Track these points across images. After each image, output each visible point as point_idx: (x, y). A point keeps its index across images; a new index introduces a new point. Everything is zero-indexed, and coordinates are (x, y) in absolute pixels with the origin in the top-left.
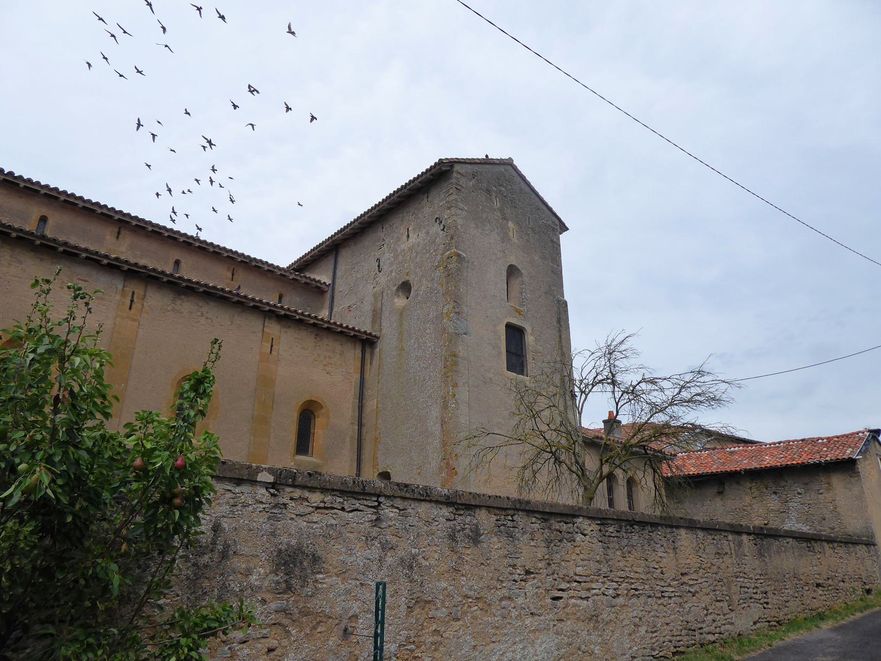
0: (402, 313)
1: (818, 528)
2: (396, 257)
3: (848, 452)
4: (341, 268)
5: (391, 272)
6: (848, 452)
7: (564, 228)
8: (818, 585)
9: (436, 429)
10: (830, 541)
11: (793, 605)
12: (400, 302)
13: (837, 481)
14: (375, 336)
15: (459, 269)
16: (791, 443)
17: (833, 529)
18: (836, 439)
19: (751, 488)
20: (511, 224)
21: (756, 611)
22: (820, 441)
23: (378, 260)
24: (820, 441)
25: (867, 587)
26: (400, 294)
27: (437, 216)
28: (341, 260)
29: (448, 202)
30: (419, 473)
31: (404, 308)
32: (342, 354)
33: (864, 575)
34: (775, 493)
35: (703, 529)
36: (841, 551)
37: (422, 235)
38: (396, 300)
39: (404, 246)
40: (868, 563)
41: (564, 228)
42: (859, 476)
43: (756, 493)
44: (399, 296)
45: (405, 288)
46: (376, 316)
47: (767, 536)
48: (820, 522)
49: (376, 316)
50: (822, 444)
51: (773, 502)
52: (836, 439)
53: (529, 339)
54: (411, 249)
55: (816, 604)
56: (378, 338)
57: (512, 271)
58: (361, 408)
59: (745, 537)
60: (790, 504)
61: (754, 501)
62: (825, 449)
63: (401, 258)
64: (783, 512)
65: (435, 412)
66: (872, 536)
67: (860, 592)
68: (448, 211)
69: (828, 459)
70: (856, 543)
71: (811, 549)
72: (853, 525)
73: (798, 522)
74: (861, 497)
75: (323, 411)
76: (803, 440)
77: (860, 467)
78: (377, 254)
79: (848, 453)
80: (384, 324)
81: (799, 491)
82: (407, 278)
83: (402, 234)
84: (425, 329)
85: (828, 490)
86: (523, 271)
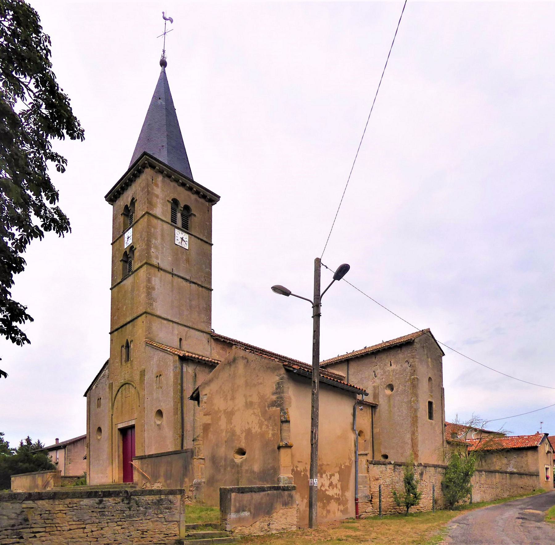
0: (389, 397)
1: (520, 470)
2: (385, 372)
3: (536, 443)
4: (351, 371)
5: (383, 378)
6: (536, 443)
7: (444, 355)
8: (522, 488)
9: (409, 441)
10: (526, 475)
11: (516, 492)
12: (388, 392)
13: (530, 453)
14: (376, 404)
15: (417, 383)
16: (513, 437)
17: (525, 470)
18: (531, 437)
19: (497, 456)
20: (429, 360)
21: (508, 493)
22: (525, 437)
23: (374, 371)
24: (525, 437)
25: (534, 489)
26: (387, 388)
27: (406, 360)
28: (350, 367)
29: (412, 355)
30: (401, 456)
31: (390, 395)
32: (366, 412)
33: (534, 486)
34: (506, 458)
35: (501, 473)
36: (529, 478)
37: (399, 366)
38: (386, 391)
39: (389, 368)
40: (536, 482)
41: (444, 355)
42: (538, 452)
43: (498, 457)
44: (386, 389)
45: (391, 387)
46: (376, 396)
47: (512, 474)
48: (521, 468)
49: (376, 396)
50: (526, 438)
51: (505, 461)
52: (531, 437)
53: (434, 406)
54: (393, 371)
55: (521, 493)
56: (378, 405)
57: (430, 379)
58: (372, 432)
59: (508, 474)
60: (511, 462)
61: (498, 460)
62: (527, 441)
63: (387, 373)
64: (508, 465)
65: (409, 436)
66: (538, 473)
67: (532, 490)
68: (412, 359)
69: (528, 446)
70: (533, 475)
71: (521, 477)
72: (532, 469)
73: (512, 468)
74: (537, 460)
75: (363, 434)
76: (518, 436)
77: (539, 449)
78: (374, 369)
79: (536, 443)
80: (380, 400)
81: (515, 457)
82: (391, 383)
83: (387, 363)
84: (402, 406)
85: (526, 457)
86: (432, 379)
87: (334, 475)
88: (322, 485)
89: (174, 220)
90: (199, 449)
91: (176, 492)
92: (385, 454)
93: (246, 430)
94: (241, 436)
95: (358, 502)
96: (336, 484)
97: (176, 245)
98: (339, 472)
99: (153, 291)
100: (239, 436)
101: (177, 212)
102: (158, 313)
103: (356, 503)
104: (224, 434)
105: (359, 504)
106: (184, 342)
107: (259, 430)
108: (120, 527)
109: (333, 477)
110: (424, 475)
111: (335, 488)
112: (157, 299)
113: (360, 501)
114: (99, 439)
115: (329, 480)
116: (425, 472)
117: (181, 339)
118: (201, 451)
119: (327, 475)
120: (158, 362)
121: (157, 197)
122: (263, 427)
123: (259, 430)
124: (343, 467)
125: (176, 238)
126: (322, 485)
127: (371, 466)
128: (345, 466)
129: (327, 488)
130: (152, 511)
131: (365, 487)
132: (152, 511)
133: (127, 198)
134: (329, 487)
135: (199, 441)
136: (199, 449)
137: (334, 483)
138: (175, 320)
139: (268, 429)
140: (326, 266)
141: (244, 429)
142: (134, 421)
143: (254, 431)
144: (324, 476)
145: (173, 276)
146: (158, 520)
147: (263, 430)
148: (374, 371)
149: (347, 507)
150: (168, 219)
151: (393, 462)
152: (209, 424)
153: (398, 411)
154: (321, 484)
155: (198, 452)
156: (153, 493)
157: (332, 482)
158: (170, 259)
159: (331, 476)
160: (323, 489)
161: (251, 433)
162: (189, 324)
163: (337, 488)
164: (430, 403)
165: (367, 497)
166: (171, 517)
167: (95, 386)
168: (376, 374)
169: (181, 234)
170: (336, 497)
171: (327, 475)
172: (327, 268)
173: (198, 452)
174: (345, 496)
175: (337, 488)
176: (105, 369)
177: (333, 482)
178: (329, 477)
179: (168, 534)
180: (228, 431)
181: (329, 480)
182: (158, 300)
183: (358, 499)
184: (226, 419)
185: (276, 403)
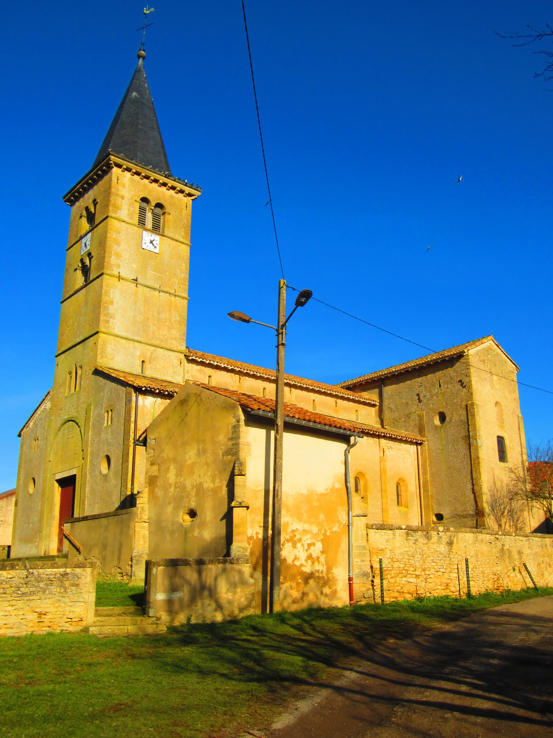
23: (418, 395)
87: (313, 544)
88: (296, 558)
89: (142, 222)
90: (143, 509)
91: (86, 565)
92: (439, 513)
93: (197, 484)
94: (191, 493)
95: (352, 583)
96: (318, 558)
97: (143, 249)
98: (322, 541)
99: (110, 306)
100: (189, 492)
101: (147, 212)
102: (116, 332)
103: (349, 583)
104: (172, 489)
105: (354, 585)
106: (147, 365)
107: (212, 485)
108: (13, 608)
109: (312, 547)
110: (454, 546)
111: (316, 563)
112: (114, 315)
113: (355, 580)
114: (30, 495)
115: (307, 550)
116: (457, 541)
117: (143, 362)
118: (144, 512)
119: (303, 545)
120: (109, 394)
121: (123, 198)
122: (216, 482)
123: (212, 485)
124: (328, 534)
125: (144, 242)
126: (296, 558)
127: (371, 532)
128: (331, 532)
129: (304, 562)
130: (54, 588)
131: (363, 561)
132: (54, 588)
133: (88, 199)
134: (306, 561)
135: (143, 498)
136: (143, 509)
137: (314, 555)
138: (137, 338)
139: (221, 484)
140: (292, 288)
141: (195, 484)
142: (75, 470)
143: (205, 486)
144: (299, 545)
145: (138, 285)
146: (60, 600)
147: (216, 485)
148: (418, 395)
149: (336, 590)
150: (136, 221)
151: (404, 527)
152: (156, 477)
153: (453, 449)
154: (293, 557)
155: (141, 513)
156: (56, 566)
157: (311, 554)
158: (134, 266)
159: (309, 545)
160: (297, 563)
161: (203, 489)
162: (157, 343)
163: (319, 562)
164: (500, 440)
165: (366, 575)
166: (77, 596)
167: (32, 421)
168: (421, 398)
169: (150, 236)
170: (317, 574)
171: (303, 545)
172: (294, 289)
173: (141, 513)
174: (332, 574)
175: (319, 562)
176: (46, 402)
177: (312, 553)
178: (306, 547)
179: (71, 619)
180: (177, 485)
181: (307, 550)
182: (116, 316)
183: (352, 578)
184: (175, 470)
185: (231, 451)
